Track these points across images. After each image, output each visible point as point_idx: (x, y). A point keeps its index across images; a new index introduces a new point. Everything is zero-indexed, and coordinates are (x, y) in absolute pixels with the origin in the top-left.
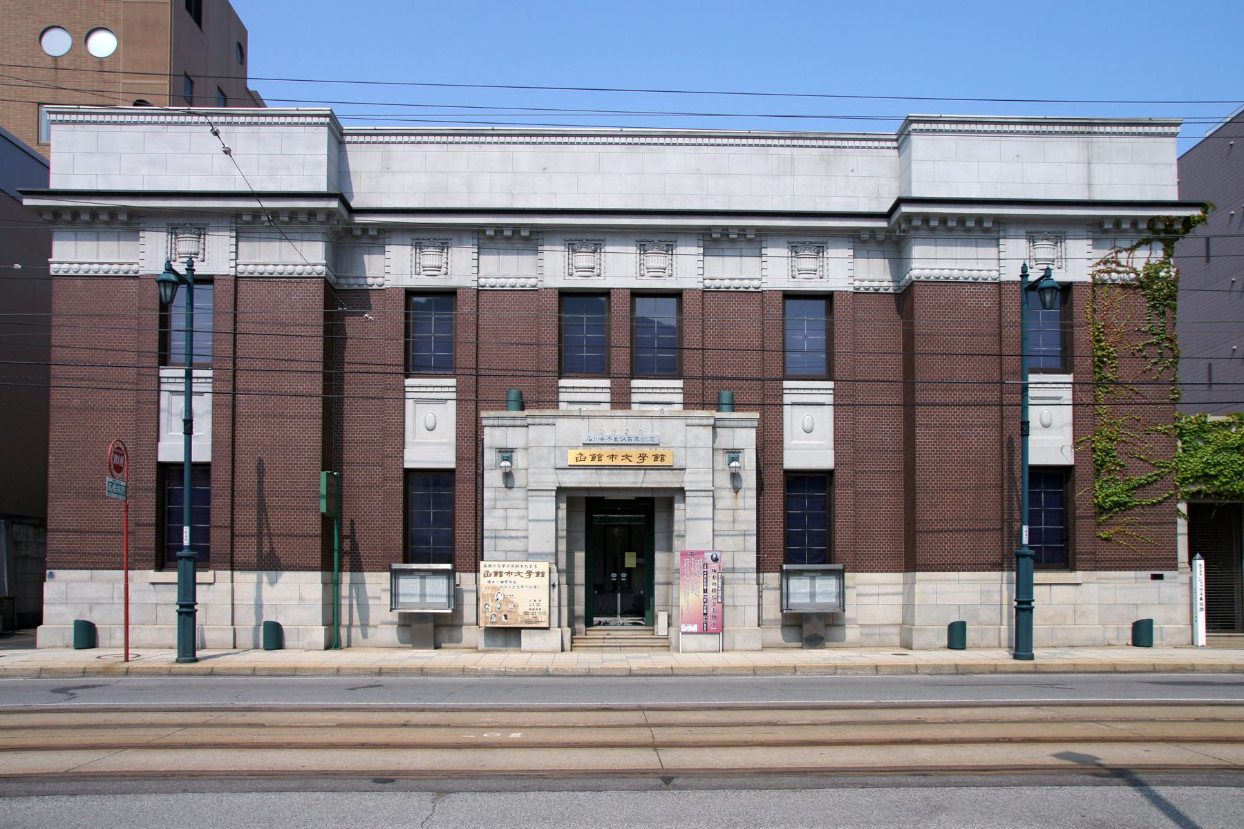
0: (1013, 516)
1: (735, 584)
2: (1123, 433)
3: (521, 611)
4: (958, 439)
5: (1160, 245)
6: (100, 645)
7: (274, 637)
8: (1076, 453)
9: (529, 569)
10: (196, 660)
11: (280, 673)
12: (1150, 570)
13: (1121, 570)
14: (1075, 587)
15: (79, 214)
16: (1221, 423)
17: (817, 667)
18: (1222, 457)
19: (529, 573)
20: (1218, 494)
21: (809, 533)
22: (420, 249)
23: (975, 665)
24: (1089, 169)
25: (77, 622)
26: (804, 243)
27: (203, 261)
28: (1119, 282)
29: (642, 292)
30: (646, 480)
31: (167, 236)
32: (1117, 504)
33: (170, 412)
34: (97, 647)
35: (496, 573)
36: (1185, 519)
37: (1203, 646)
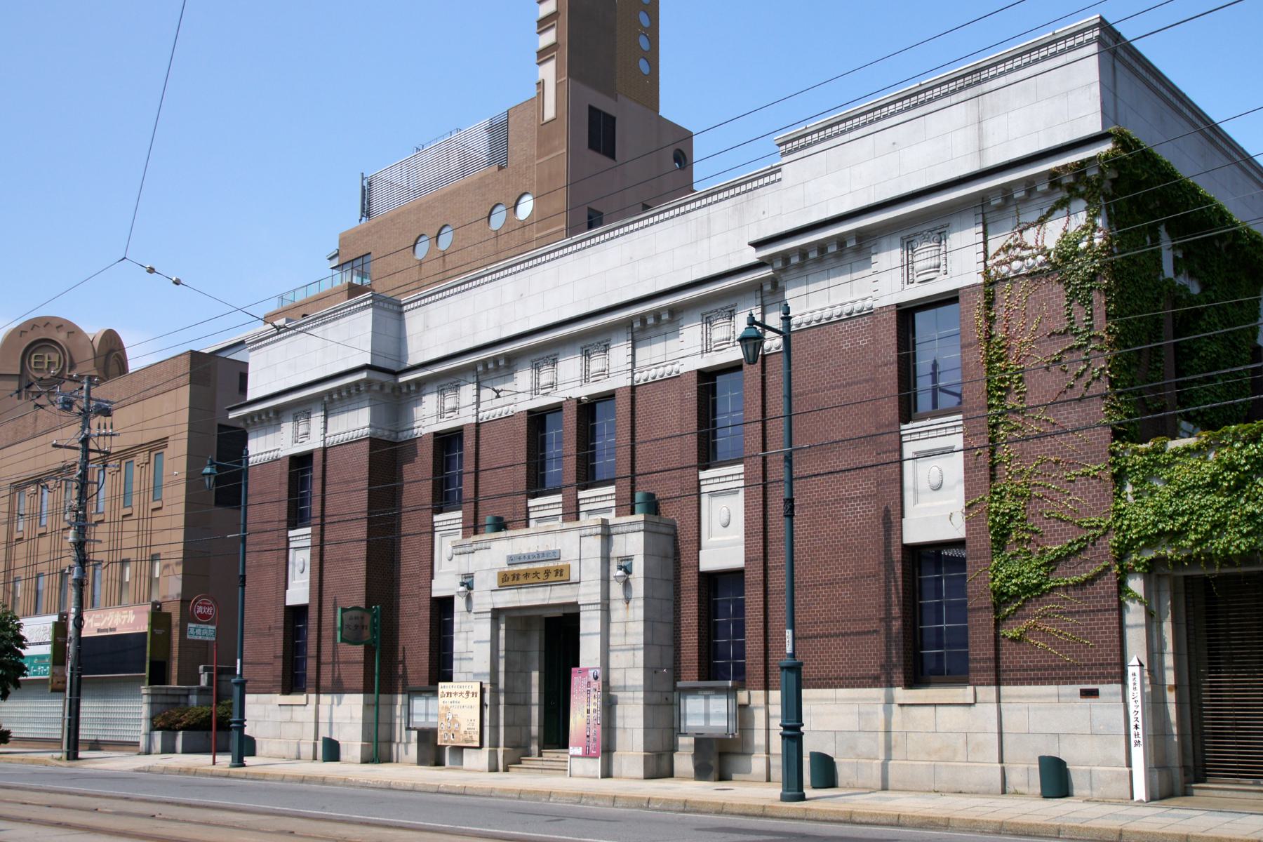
0: (891, 613)
1: (627, 704)
2: (1035, 485)
3: (463, 730)
4: (833, 519)
5: (1082, 204)
6: (839, 785)
7: (332, 751)
8: (967, 522)
9: (467, 690)
10: (244, 766)
11: (258, 777)
12: (1079, 683)
13: (1036, 684)
14: (966, 708)
15: (845, 242)
16: (1187, 449)
17: (568, 794)
18: (1194, 500)
19: (468, 693)
20: (1192, 560)
21: (734, 642)
22: (710, 324)
23: (703, 803)
24: (980, 129)
25: (1042, 760)
26: (716, 311)
27: (946, 274)
28: (1024, 271)
29: (723, 367)
30: (552, 595)
31: (902, 253)
32: (1026, 589)
33: (294, 564)
34: (1072, 796)
35: (448, 694)
36: (1141, 602)
37: (1141, 801)
